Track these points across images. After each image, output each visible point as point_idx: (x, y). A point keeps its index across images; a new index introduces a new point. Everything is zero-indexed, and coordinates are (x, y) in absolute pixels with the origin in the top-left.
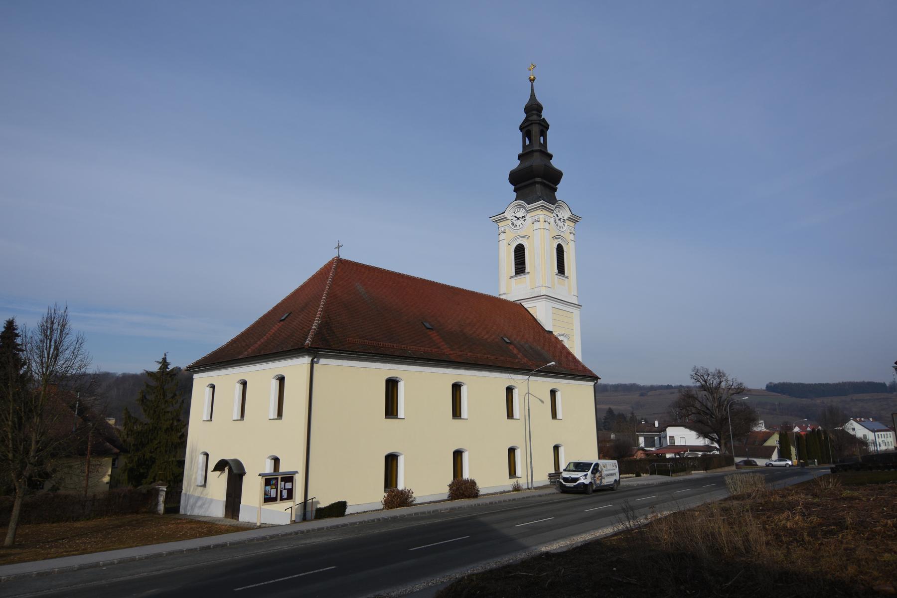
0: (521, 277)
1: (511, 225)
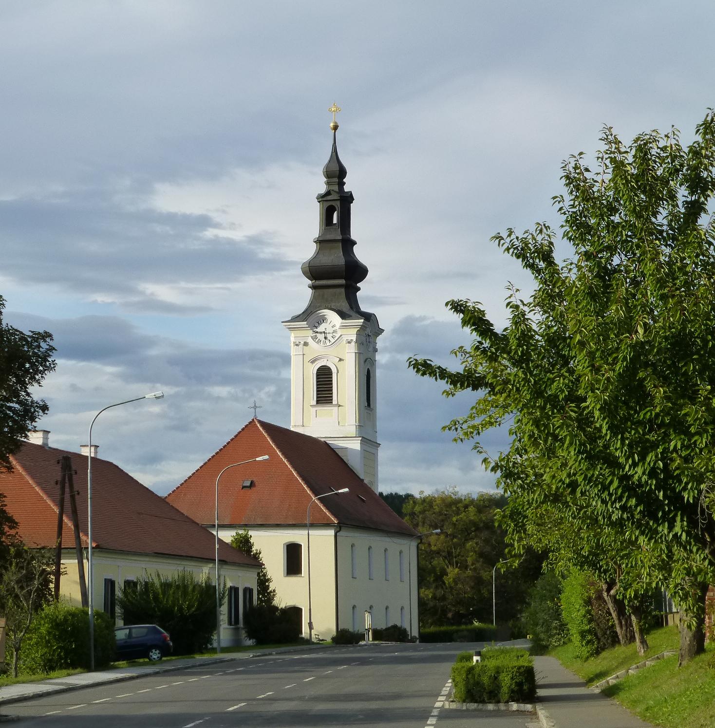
0: (324, 409)
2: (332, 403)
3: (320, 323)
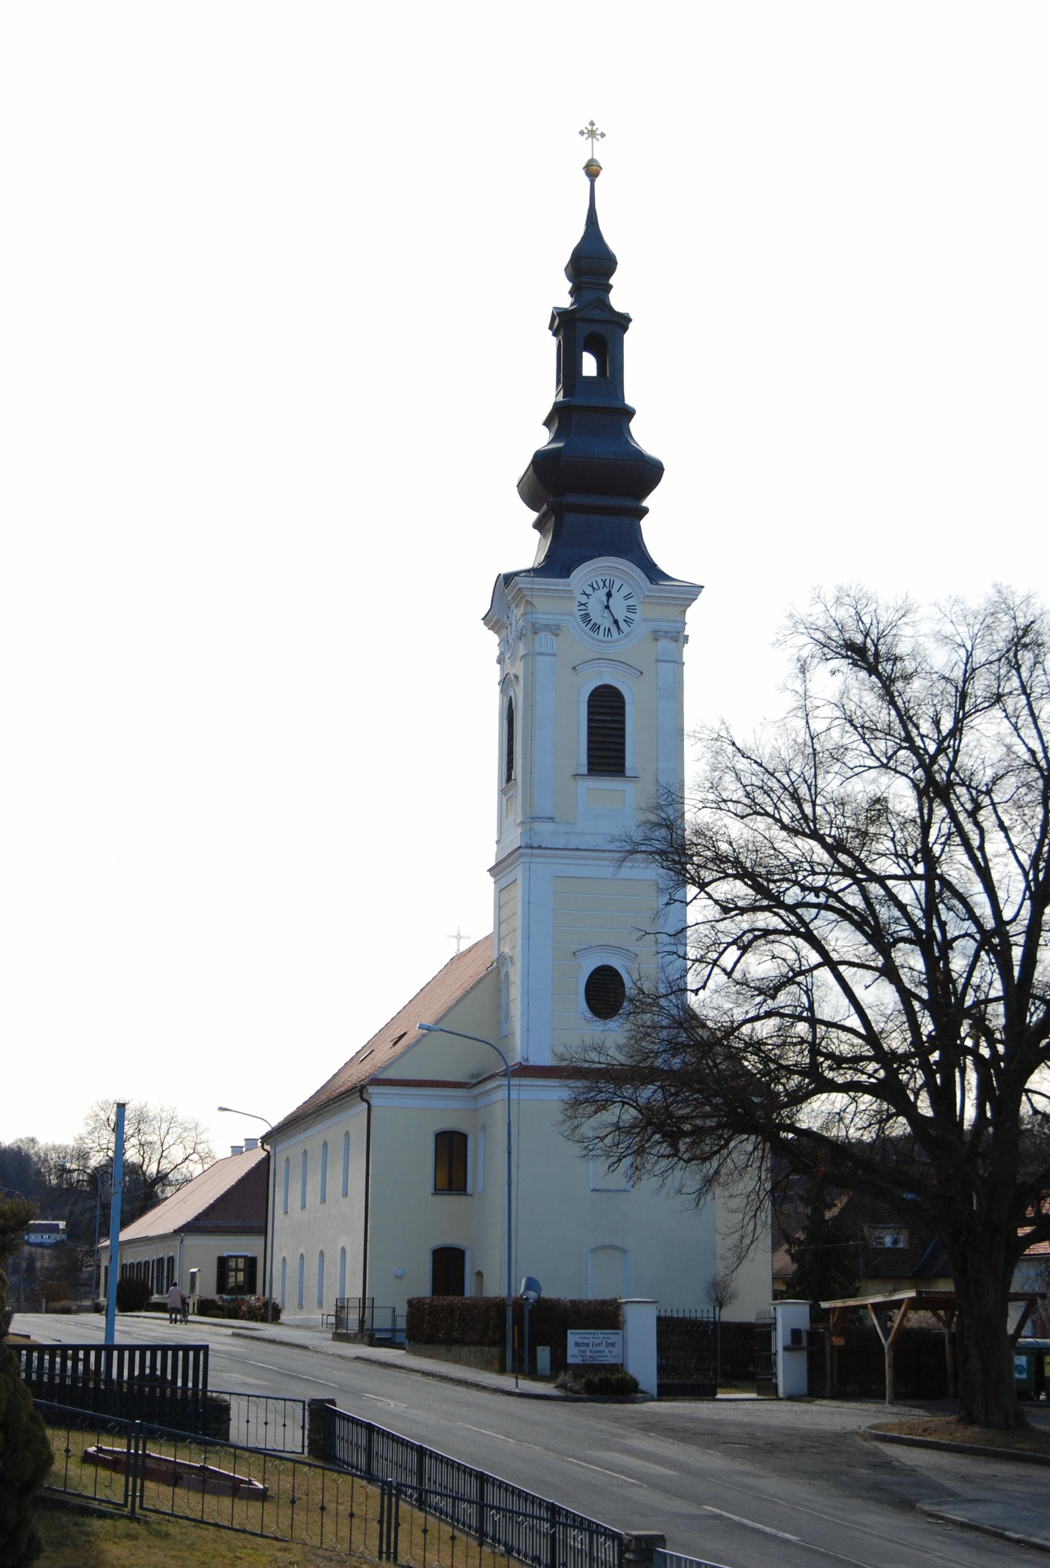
3: (595, 586)
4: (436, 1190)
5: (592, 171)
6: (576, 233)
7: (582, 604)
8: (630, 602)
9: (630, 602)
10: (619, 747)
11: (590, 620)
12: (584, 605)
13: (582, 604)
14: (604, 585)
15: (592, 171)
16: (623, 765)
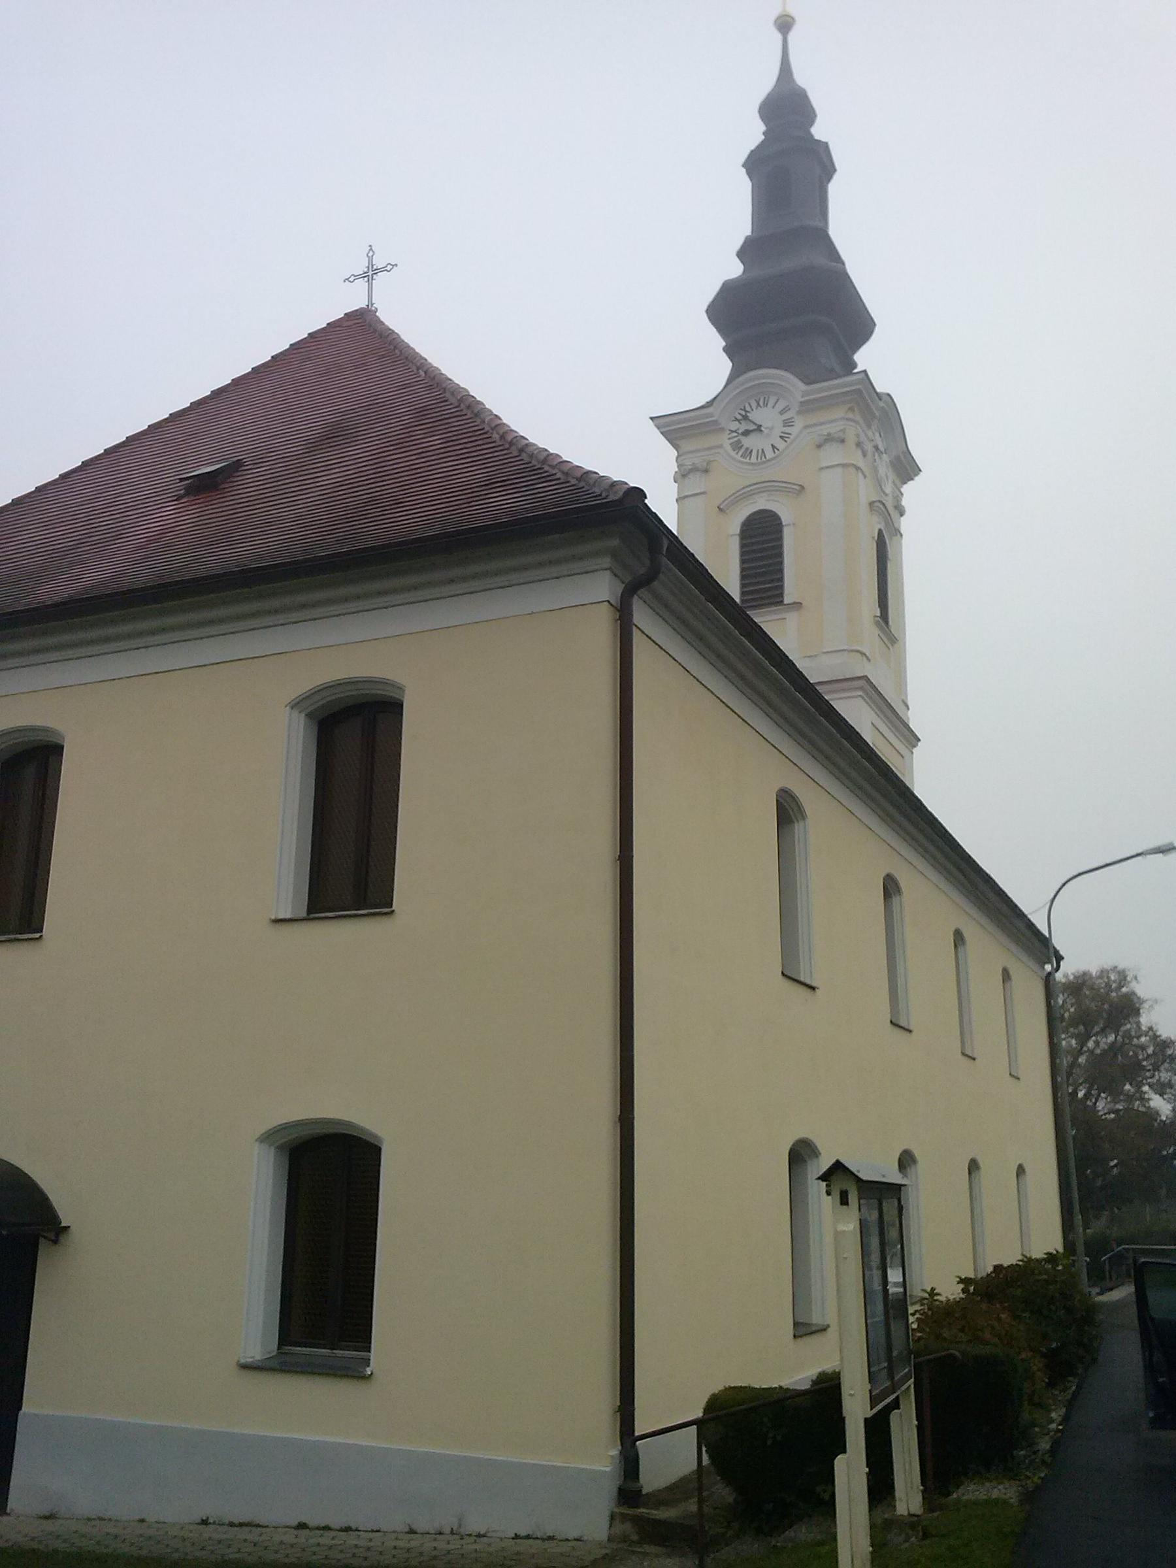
1: (729, 448)
2: (782, 601)
4: (286, 1337)
5: (785, 25)
6: (766, 83)
7: (732, 431)
8: (786, 416)
9: (786, 416)
10: (745, 566)
11: (742, 446)
12: (735, 432)
13: (732, 431)
14: (758, 404)
15: (785, 25)
16: (781, 595)
